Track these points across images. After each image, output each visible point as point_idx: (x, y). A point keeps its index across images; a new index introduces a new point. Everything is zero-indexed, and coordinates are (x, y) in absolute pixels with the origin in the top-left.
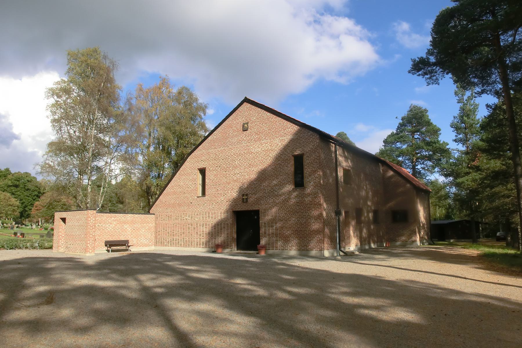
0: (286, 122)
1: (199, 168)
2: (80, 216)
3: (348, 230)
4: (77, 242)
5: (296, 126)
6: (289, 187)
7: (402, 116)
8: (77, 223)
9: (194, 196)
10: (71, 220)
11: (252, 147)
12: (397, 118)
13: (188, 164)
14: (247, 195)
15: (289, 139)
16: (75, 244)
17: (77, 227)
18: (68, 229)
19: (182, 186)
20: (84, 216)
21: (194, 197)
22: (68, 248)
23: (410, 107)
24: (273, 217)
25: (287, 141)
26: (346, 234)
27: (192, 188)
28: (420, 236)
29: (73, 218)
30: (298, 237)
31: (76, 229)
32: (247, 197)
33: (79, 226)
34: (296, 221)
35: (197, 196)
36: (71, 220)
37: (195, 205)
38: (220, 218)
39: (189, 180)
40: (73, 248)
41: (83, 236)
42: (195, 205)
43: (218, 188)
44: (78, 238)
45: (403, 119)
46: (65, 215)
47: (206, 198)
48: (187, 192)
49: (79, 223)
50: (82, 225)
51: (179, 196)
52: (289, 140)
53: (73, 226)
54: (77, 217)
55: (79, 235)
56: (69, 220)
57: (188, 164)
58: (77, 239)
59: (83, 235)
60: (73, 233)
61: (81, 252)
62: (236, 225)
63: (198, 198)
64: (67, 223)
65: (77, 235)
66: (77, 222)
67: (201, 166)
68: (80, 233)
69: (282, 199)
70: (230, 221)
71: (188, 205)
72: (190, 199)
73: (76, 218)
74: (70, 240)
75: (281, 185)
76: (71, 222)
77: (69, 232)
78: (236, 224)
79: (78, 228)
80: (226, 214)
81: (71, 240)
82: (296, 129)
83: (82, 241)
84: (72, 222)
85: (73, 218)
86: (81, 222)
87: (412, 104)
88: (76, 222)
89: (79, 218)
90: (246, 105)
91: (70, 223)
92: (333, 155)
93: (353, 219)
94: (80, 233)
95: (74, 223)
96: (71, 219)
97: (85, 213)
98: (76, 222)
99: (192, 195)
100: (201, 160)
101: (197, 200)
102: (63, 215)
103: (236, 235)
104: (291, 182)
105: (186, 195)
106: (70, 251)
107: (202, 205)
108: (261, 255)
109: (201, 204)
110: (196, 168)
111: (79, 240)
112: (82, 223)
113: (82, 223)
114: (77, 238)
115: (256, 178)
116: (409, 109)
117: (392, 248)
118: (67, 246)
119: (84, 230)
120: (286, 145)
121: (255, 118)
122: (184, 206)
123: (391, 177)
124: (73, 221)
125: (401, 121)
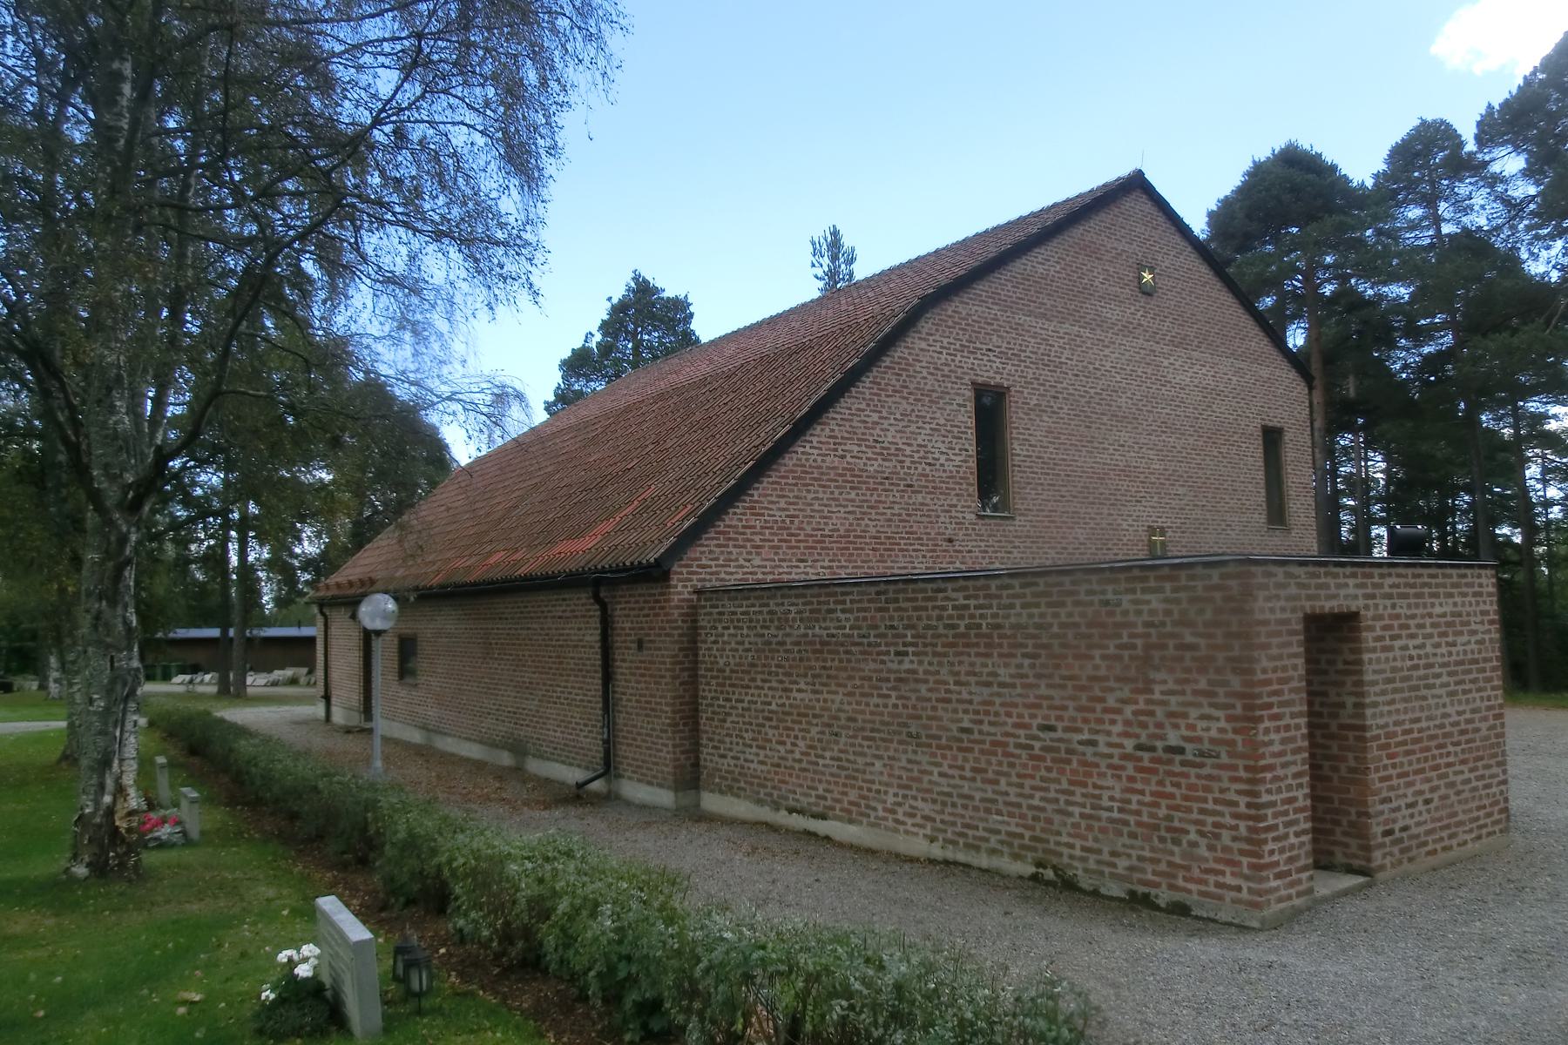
1: (980, 380)
2: (1455, 604)
4: (1456, 773)
8: (1444, 650)
9: (959, 508)
10: (1402, 627)
11: (1166, 363)
13: (923, 345)
14: (1163, 532)
16: (1443, 791)
17: (1445, 679)
18: (1389, 697)
19: (893, 447)
20: (1478, 603)
21: (960, 515)
22: (1397, 835)
27: (949, 466)
29: (1413, 617)
30: (681, 693)
31: (1443, 691)
33: (1460, 668)
36: (1404, 633)
37: (970, 551)
39: (933, 426)
40: (1430, 826)
41: (1484, 732)
42: (970, 551)
43: (1064, 489)
44: (1458, 749)
46: (1351, 591)
47: (1017, 523)
48: (923, 483)
49: (1454, 649)
50: (1476, 661)
51: (879, 496)
53: (1415, 673)
54: (1438, 610)
55: (1463, 726)
56: (1384, 628)
57: (923, 345)
58: (1451, 759)
59: (1484, 725)
60: (1424, 724)
61: (1484, 831)
63: (980, 522)
64: (1374, 650)
65: (1448, 729)
66: (1444, 640)
67: (991, 372)
68: (1468, 716)
71: (934, 551)
72: (942, 519)
73: (1430, 615)
74: (1406, 774)
76: (1397, 643)
77: (1390, 720)
79: (1452, 680)
81: (1416, 772)
83: (1480, 764)
84: (1411, 643)
85: (1413, 617)
86: (1465, 638)
88: (1437, 645)
89: (1453, 614)
91: (1398, 653)
94: (1464, 712)
95: (1422, 652)
96: (1396, 623)
97: (1481, 585)
98: (1436, 639)
99: (948, 502)
100: (984, 347)
101: (974, 529)
102: (1333, 591)
105: (920, 498)
106: (1414, 852)
107: (999, 555)
109: (996, 552)
110: (967, 377)
111: (1463, 762)
112: (1474, 646)
113: (1474, 646)
114: (1451, 749)
118: (1386, 822)
119: (1484, 689)
122: (914, 554)
124: (1412, 636)
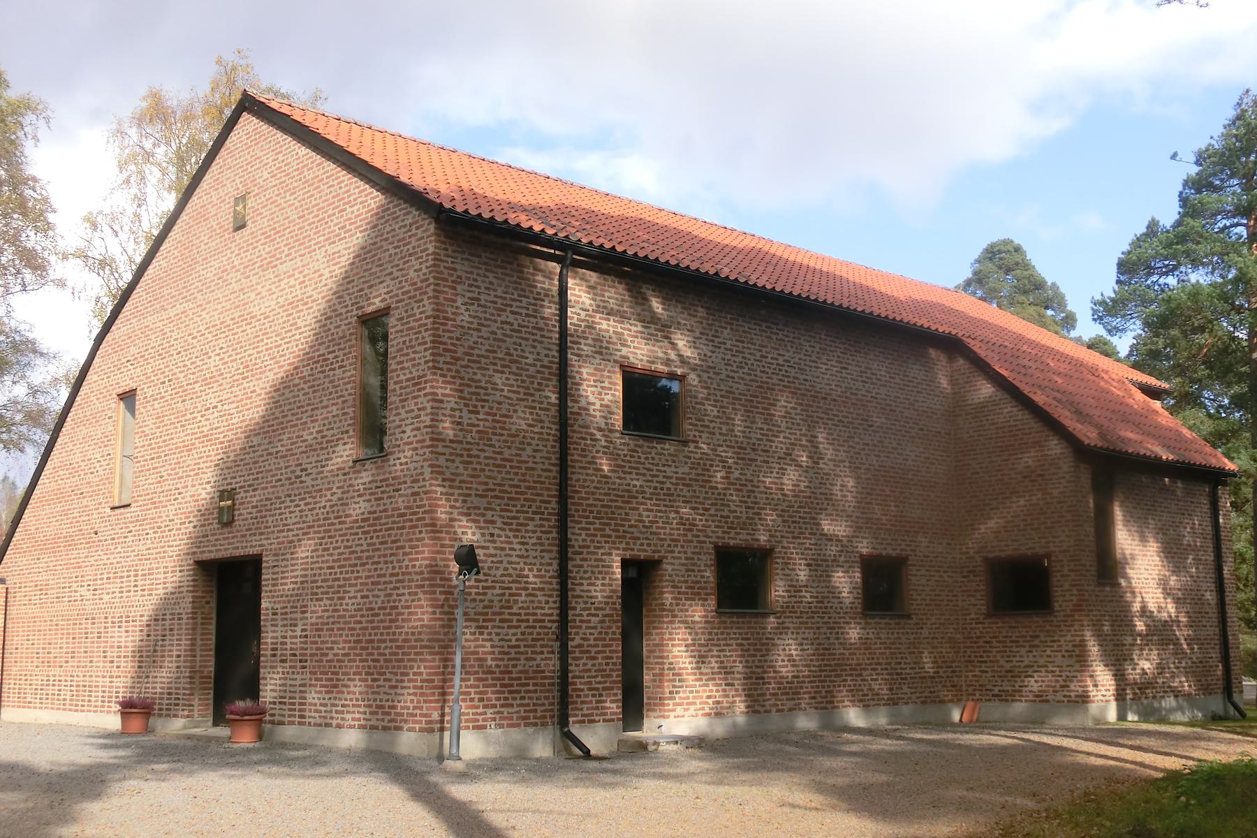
0: (349, 179)
3: (657, 645)
5: (375, 193)
6: (346, 452)
7: (1196, 149)
11: (252, 295)
12: (1174, 156)
15: (351, 250)
23: (1239, 104)
24: (296, 583)
25: (347, 257)
26: (652, 660)
28: (1120, 676)
32: (229, 502)
34: (359, 600)
35: (112, 505)
38: (161, 592)
45: (1200, 158)
52: (351, 256)
62: (214, 622)
69: (324, 507)
70: (186, 605)
75: (326, 445)
78: (214, 615)
80: (178, 574)
82: (373, 206)
87: (1248, 91)
90: (248, 123)
92: (550, 310)
93: (695, 593)
103: (212, 663)
104: (351, 433)
108: (236, 746)
115: (258, 423)
116: (1231, 113)
117: (961, 732)
120: (343, 275)
121: (266, 175)
123: (982, 407)
125: (1194, 170)
